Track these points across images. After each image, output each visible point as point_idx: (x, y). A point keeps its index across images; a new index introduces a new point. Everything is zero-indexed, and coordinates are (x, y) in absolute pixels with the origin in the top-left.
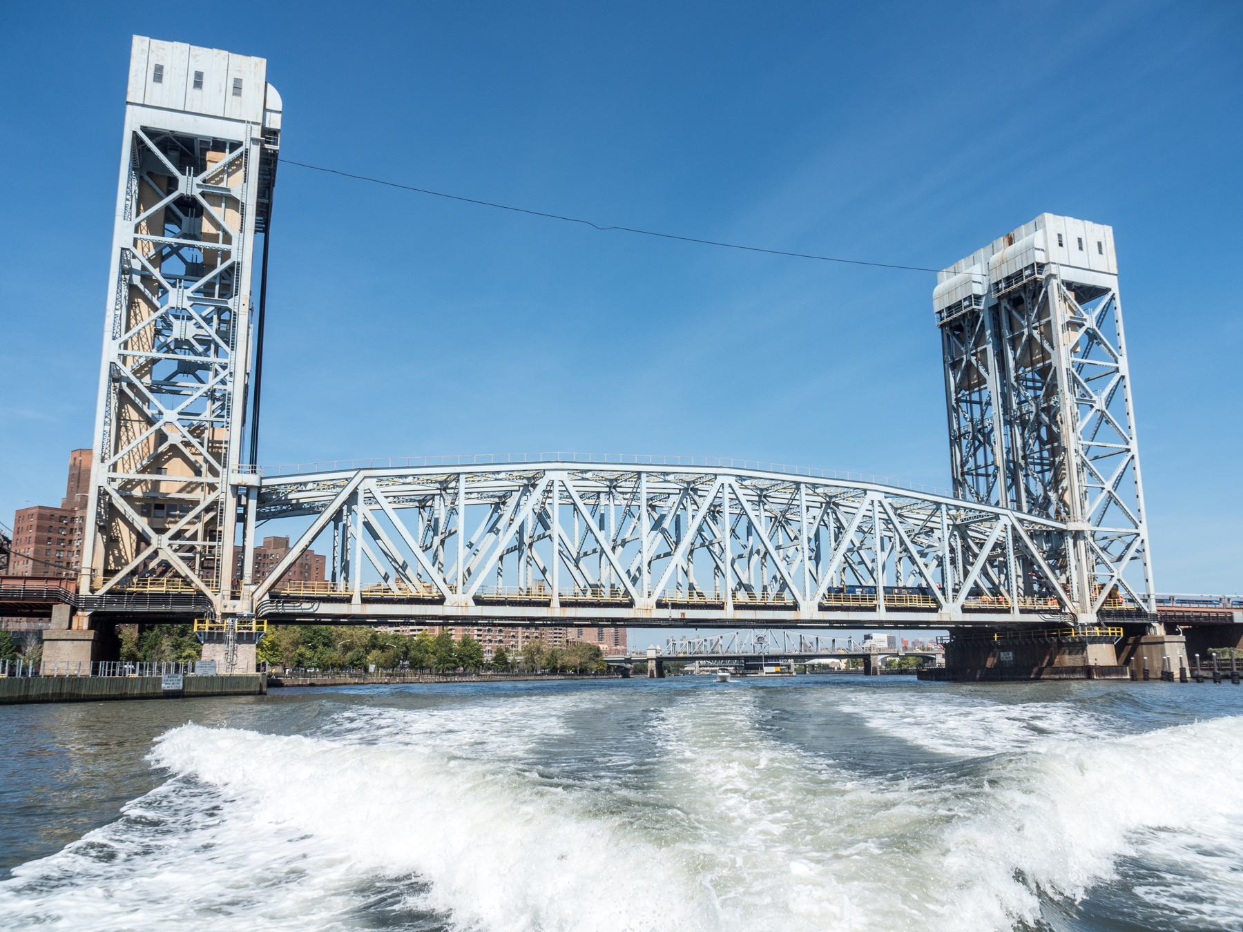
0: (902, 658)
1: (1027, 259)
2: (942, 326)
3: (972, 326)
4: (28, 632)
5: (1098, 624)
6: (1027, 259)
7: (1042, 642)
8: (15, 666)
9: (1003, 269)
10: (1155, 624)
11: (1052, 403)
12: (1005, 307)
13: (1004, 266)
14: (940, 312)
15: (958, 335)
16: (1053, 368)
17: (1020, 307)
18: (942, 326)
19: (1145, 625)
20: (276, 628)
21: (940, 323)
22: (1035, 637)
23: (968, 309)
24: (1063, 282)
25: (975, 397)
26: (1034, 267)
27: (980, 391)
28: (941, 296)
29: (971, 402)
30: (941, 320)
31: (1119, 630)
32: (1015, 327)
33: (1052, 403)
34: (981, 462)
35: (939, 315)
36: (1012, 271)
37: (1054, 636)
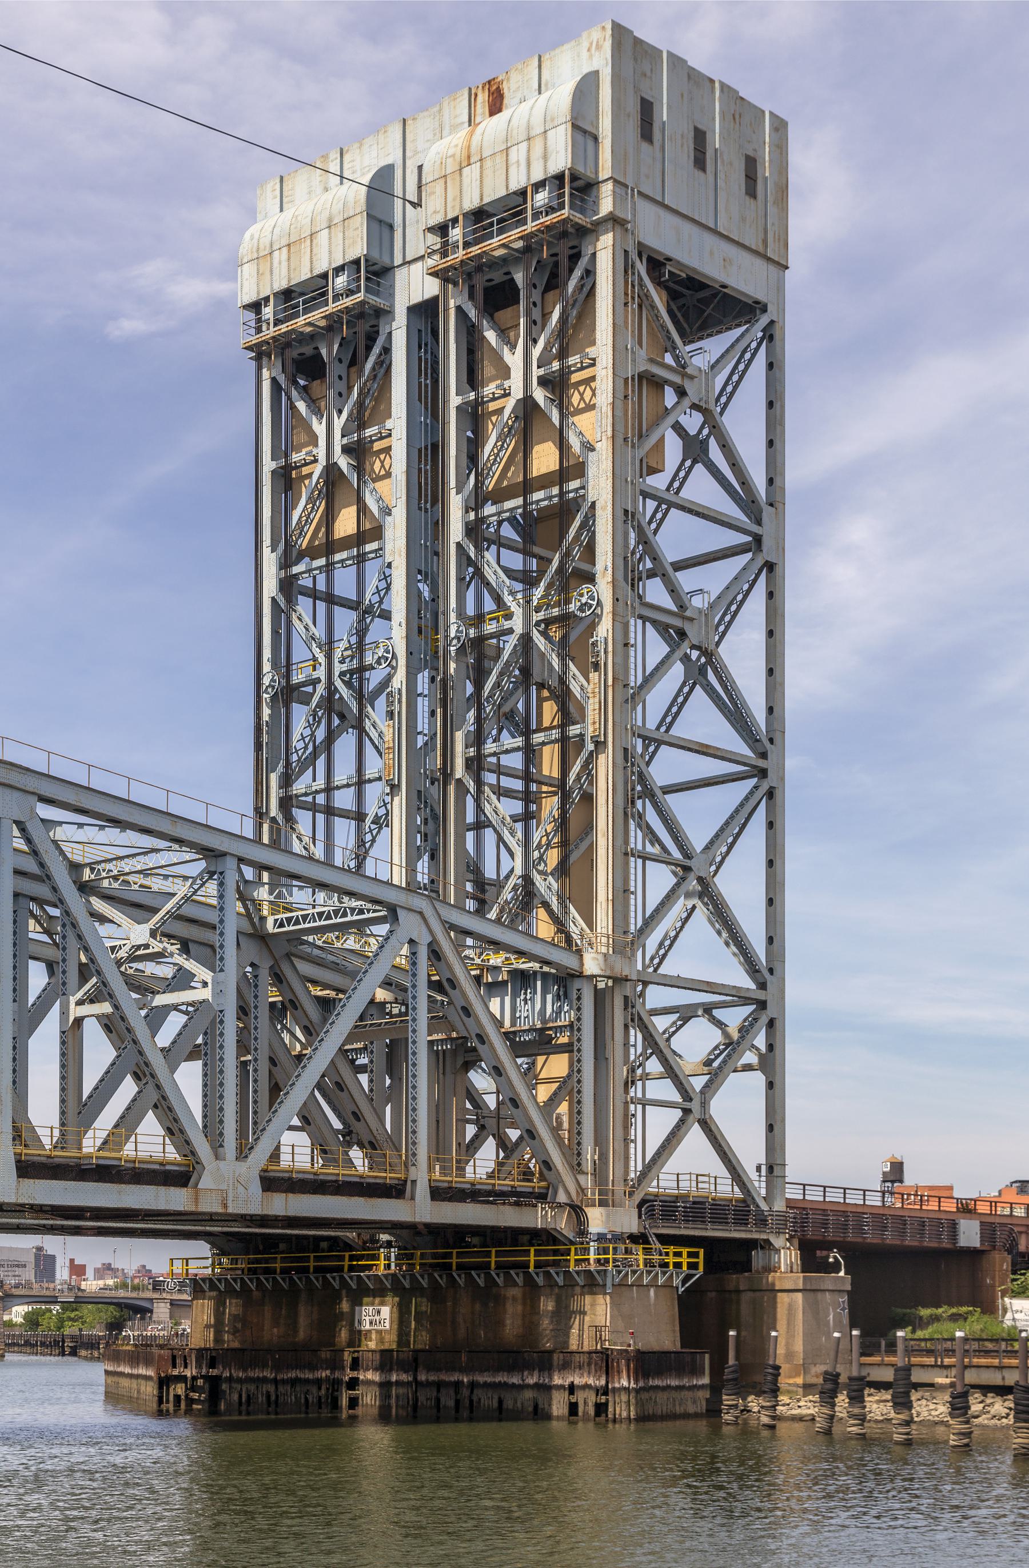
0: (66, 1306)
1: (545, 158)
2: (260, 353)
3: (353, 362)
4: (535, 973)
5: (639, 1238)
6: (545, 158)
7: (481, 1282)
8: (347, 308)
9: (466, 181)
10: (778, 1241)
11: (572, 607)
12: (459, 309)
13: (471, 173)
14: (256, 307)
15: (305, 387)
16: (585, 509)
17: (504, 315)
18: (260, 353)
19: (751, 1245)
20: (208, 1326)
21: (254, 339)
22: (460, 1267)
23: (348, 302)
24: (642, 249)
25: (345, 584)
26: (561, 186)
27: (361, 559)
28: (264, 257)
29: (331, 599)
30: (259, 330)
31: (695, 1255)
32: (488, 369)
33: (572, 607)
34: (345, 771)
35: (251, 316)
36: (495, 191)
37: (478, 1267)
